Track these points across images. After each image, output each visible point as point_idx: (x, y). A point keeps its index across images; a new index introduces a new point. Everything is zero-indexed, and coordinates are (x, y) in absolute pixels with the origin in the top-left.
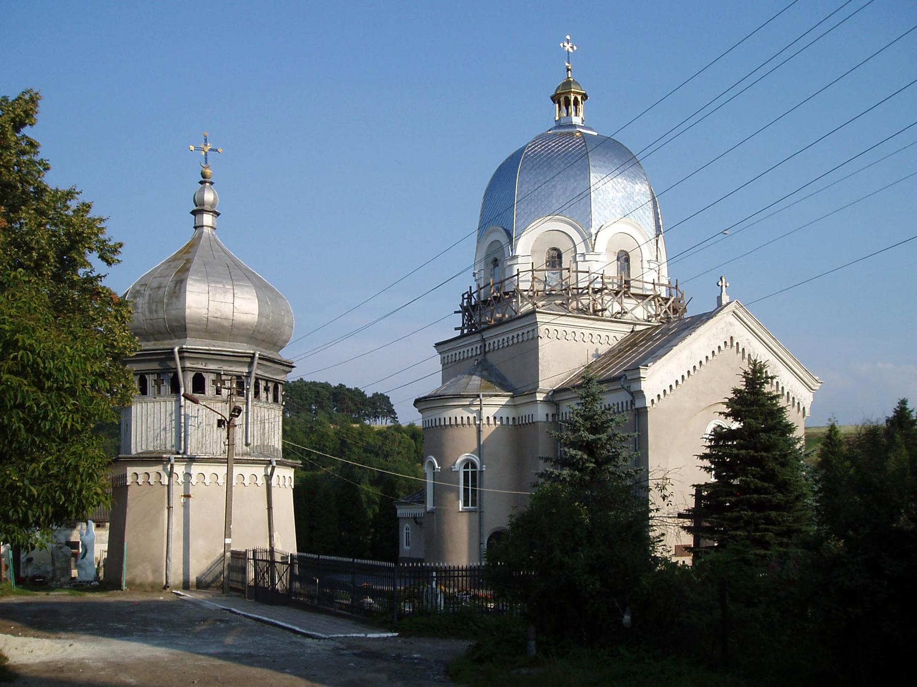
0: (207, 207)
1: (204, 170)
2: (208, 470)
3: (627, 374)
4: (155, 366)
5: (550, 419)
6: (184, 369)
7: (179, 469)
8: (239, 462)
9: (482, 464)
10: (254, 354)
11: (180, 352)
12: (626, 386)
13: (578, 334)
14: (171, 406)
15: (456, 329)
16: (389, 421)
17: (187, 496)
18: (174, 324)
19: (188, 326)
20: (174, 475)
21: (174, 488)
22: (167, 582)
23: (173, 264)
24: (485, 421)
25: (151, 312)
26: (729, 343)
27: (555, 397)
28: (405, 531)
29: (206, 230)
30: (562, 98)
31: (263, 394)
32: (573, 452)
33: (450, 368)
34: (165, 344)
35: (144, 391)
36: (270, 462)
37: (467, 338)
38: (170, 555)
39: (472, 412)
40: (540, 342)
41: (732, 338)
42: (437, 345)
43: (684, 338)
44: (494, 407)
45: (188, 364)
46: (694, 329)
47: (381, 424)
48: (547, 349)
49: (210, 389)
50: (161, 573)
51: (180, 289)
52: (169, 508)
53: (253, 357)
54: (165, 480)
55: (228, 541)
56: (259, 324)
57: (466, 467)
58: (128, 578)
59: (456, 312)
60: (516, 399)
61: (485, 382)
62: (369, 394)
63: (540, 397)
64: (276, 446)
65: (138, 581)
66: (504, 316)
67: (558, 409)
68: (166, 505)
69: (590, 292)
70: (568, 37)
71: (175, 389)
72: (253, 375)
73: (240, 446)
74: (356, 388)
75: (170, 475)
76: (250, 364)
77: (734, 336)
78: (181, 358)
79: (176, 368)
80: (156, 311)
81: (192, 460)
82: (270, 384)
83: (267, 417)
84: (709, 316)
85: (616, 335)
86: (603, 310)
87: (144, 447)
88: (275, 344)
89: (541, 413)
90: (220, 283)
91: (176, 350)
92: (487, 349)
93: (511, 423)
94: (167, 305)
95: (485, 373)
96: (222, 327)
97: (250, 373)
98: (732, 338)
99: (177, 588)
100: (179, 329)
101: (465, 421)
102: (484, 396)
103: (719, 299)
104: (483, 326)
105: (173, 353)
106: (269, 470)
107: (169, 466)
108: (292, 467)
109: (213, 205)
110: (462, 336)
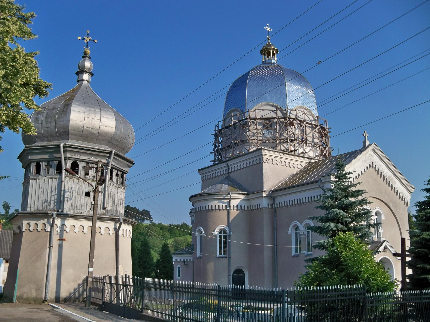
0: (85, 70)
1: (86, 50)
2: (78, 223)
3: (322, 179)
4: (46, 156)
5: (270, 207)
6: (66, 158)
7: (58, 222)
8: (100, 219)
9: (230, 231)
10: (112, 151)
11: (64, 147)
12: (321, 186)
13: (283, 162)
14: (55, 182)
15: (211, 161)
16: (149, 222)
17: (62, 239)
18: (62, 130)
19: (70, 131)
20: (55, 226)
21: (55, 232)
22: (45, 297)
23: (63, 98)
24: (232, 208)
25: (47, 122)
26: (371, 166)
27: (273, 194)
28: (177, 269)
29: (84, 82)
30: (266, 52)
31: (115, 178)
32: (338, 211)
33: (205, 182)
34: (55, 143)
35: (38, 171)
36: (119, 220)
37: (217, 166)
38: (49, 279)
39: (224, 203)
40: (264, 165)
41: (372, 163)
42: (199, 170)
43: (351, 161)
44: (237, 199)
45: (68, 155)
46: (356, 157)
47: (146, 223)
48: (267, 168)
49: (81, 172)
50: (42, 290)
51: (67, 109)
52: (50, 247)
53: (110, 153)
54: (48, 229)
55: (91, 270)
56: (115, 134)
57: (220, 232)
58: (18, 294)
59: (211, 153)
60: (250, 196)
61: (231, 188)
62: (141, 210)
63: (265, 194)
64: (121, 211)
65: (25, 296)
66: (240, 152)
67: (274, 201)
68: (48, 245)
69: (289, 140)
70: (268, 25)
71: (59, 168)
72: (110, 165)
73: (100, 210)
74: (135, 207)
75: (52, 225)
76: (109, 157)
77: (374, 162)
78: (65, 151)
79: (61, 158)
80: (51, 123)
81: (67, 216)
82: (119, 173)
83: (116, 193)
84: (361, 151)
85: (302, 164)
86: (295, 150)
87: (36, 209)
88: (123, 149)
89: (265, 203)
90: (92, 107)
91: (62, 145)
92: (230, 171)
93: (246, 209)
94: (58, 119)
95: (230, 183)
96: (92, 134)
97: (108, 163)
98: (372, 163)
99: (52, 302)
100: (65, 133)
101: (221, 207)
102: (232, 194)
103: (365, 142)
104: (227, 159)
105: (59, 147)
106: (118, 225)
107: (51, 220)
108: (132, 224)
109: (89, 69)
110: (215, 165)
